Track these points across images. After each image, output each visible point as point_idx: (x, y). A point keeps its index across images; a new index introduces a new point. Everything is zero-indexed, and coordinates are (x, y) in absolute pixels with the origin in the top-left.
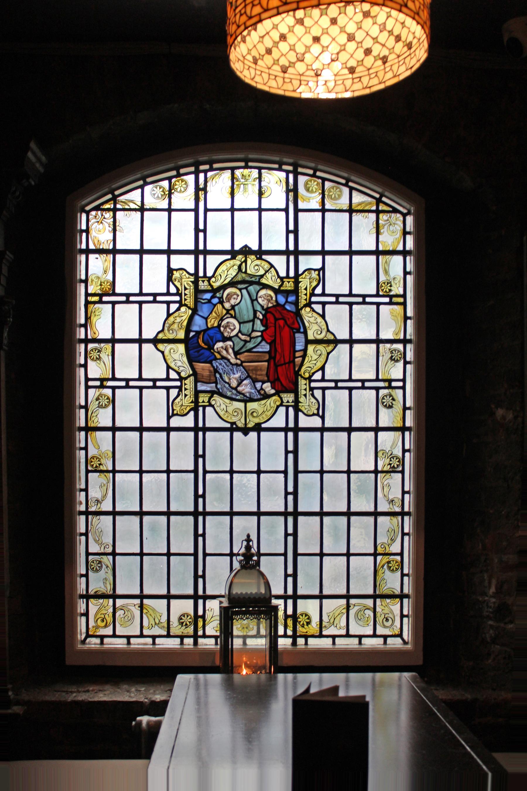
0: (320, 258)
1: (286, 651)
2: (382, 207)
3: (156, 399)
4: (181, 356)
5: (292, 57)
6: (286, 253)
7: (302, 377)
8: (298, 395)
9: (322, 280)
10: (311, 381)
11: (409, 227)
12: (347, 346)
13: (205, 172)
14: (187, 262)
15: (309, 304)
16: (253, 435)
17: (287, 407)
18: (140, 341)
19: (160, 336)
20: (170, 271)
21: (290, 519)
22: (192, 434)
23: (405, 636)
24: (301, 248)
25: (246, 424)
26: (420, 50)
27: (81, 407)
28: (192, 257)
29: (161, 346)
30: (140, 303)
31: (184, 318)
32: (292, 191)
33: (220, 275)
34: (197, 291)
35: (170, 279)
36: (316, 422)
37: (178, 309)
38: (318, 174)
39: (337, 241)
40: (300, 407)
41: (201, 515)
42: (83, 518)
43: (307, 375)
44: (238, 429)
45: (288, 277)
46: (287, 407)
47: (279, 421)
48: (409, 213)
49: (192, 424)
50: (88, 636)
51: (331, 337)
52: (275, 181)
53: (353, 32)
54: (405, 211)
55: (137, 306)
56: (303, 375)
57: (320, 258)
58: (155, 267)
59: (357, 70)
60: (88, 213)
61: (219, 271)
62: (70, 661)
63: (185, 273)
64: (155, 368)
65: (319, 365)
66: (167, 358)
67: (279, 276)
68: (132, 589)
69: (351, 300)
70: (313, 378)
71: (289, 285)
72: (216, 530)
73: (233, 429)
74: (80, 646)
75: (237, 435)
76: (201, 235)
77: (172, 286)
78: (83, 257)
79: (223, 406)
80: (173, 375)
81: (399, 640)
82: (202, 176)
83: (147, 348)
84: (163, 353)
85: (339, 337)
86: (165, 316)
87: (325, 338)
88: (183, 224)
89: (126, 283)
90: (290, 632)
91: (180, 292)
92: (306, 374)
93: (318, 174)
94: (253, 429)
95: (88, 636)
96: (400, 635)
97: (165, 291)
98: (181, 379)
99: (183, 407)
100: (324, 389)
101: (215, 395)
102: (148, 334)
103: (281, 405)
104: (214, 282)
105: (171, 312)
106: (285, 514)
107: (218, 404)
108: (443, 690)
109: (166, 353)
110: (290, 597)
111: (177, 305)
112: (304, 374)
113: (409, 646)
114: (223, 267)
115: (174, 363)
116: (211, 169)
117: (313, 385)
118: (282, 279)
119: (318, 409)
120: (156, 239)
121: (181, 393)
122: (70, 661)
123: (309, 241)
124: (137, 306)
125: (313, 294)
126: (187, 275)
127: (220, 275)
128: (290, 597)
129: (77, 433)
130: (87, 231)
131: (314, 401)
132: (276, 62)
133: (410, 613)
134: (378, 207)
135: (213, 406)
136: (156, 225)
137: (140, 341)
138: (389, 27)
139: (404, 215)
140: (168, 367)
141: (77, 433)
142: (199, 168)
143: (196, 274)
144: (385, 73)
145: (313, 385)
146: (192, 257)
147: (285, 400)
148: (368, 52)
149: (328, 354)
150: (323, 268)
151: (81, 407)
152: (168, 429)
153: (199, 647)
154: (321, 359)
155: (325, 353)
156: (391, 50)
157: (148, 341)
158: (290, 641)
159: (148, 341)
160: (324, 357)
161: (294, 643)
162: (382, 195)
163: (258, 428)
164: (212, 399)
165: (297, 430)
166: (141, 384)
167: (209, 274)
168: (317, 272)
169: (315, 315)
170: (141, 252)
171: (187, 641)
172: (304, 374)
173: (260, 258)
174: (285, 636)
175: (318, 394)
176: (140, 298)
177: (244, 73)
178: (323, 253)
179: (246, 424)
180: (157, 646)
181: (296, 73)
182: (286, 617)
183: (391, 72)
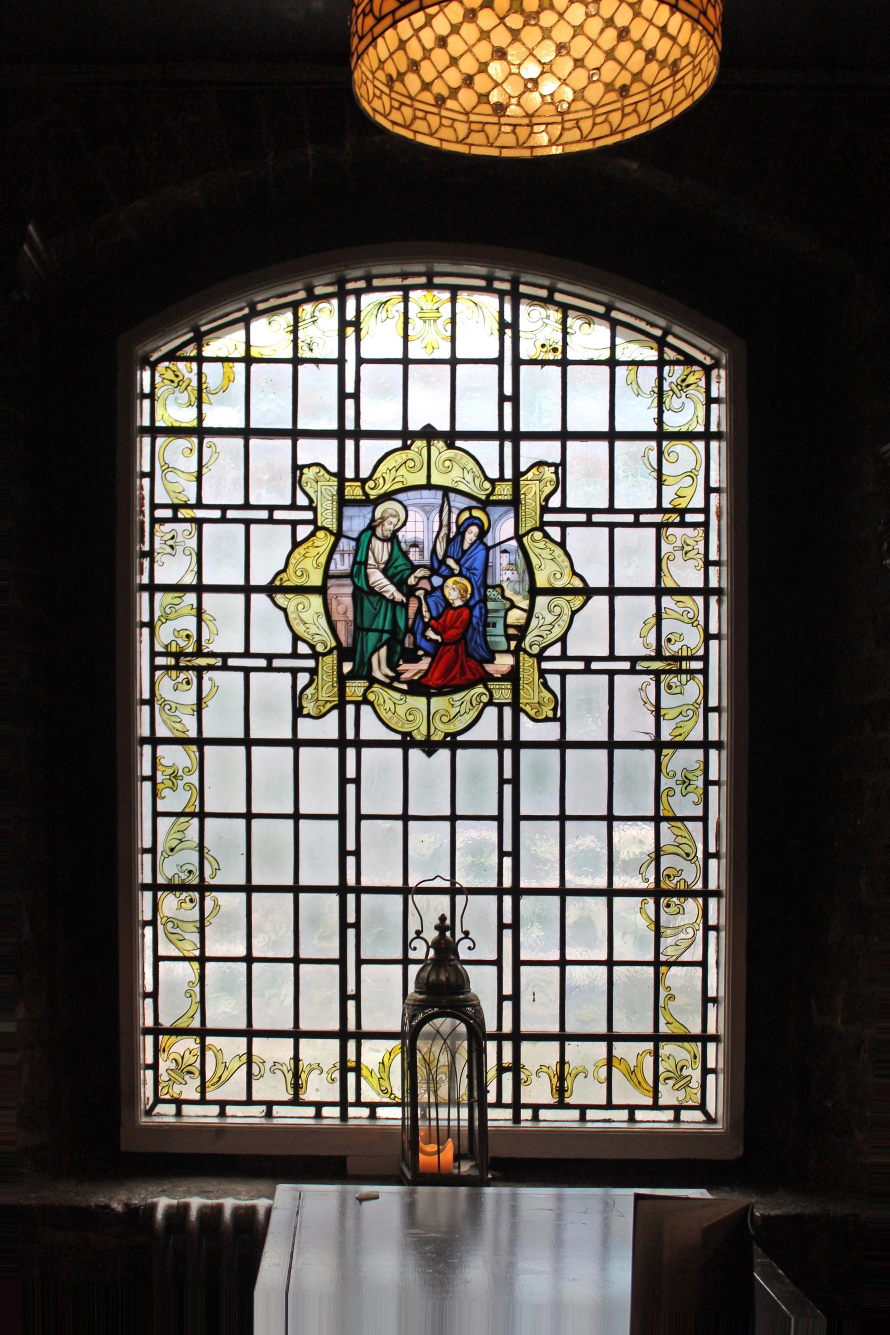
0: (301, 735)
1: (501, 1133)
2: (670, 355)
3: (273, 689)
4: (316, 616)
6: (499, 436)
7: (526, 652)
8: (519, 685)
9: (561, 483)
10: (314, 522)
11: (719, 389)
12: (605, 599)
13: (358, 293)
14: (324, 452)
15: (542, 526)
16: (444, 754)
17: (357, 478)
18: (247, 590)
19: (578, 601)
20: (297, 469)
21: (508, 900)
22: (334, 752)
23: (711, 1107)
24: (523, 428)
25: (429, 735)
28: (333, 443)
29: (280, 598)
30: (612, 657)
31: (321, 550)
32: (509, 327)
33: (384, 478)
34: (343, 502)
35: (296, 482)
36: (551, 732)
37: (313, 534)
38: (558, 297)
39: (588, 414)
40: (521, 705)
41: (351, 892)
42: (148, 896)
43: (535, 650)
44: (441, 435)
45: (358, 705)
46: (500, 706)
47: (486, 730)
48: (717, 365)
49: (334, 735)
50: (158, 1100)
51: (578, 583)
52: (479, 314)
54: (708, 361)
55: (618, 653)
56: (528, 649)
57: (557, 444)
58: (585, 724)
59: (632, 91)
60: (153, 366)
61: (473, 714)
62: (125, 1146)
63: (323, 472)
64: (271, 636)
65: (557, 632)
66: (567, 563)
67: (487, 478)
68: (242, 1000)
69: (607, 518)
70: (546, 654)
71: (355, 689)
72: (381, 915)
73: (451, 437)
74: (144, 1120)
75: (415, 754)
76: (508, 774)
77: (300, 495)
78: (147, 441)
79: (389, 705)
80: (555, 533)
81: (698, 1115)
82: (351, 302)
83: (259, 600)
84: (285, 610)
85: (592, 584)
86: (289, 547)
87: (569, 586)
88: (319, 385)
89: (223, 488)
90: (507, 1098)
91: (314, 505)
92: (534, 647)
93: (558, 297)
94: (442, 744)
95: (158, 1100)
96: (702, 1107)
97: (288, 502)
98: (315, 655)
99: (319, 703)
100: (563, 673)
101: (375, 685)
102: (260, 578)
103: (490, 703)
104: (372, 489)
105: (299, 539)
106: (499, 892)
107: (477, 482)
109: (568, 571)
110: (507, 1037)
111: (310, 528)
112: (530, 647)
113: (719, 1127)
114: (390, 462)
115: (555, 554)
116: (370, 289)
117: (545, 665)
118: (493, 482)
119: (555, 710)
120: (271, 411)
121: (543, 503)
122: (125, 1146)
123: (321, 765)
124: (618, 653)
125: (545, 509)
126: (327, 476)
127: (384, 478)
128: (507, 1037)
130: (152, 396)
131: (548, 695)
132: (483, 98)
134: (661, 353)
135: (371, 704)
136: (271, 383)
137: (247, 590)
139: (707, 371)
140: (562, 545)
142: (344, 287)
143: (340, 475)
145: (545, 665)
146: (333, 443)
147: (496, 695)
148: (650, 55)
149: (574, 613)
150: (564, 462)
152: (564, 436)
153: (351, 1122)
154: (561, 622)
155: (567, 613)
157: (259, 589)
158: (508, 1113)
159: (259, 589)
160: (566, 618)
161: (517, 1119)
162: (666, 332)
163: (453, 743)
164: (488, 492)
165: (517, 745)
166: (249, 662)
167: (364, 474)
168: (552, 469)
169: (550, 545)
170: (611, 745)
171: (326, 1111)
172: (530, 647)
173: (404, 734)
174: (499, 1104)
175: (554, 681)
176: (246, 515)
178: (296, 743)
179: (429, 735)
180: (275, 1121)
181: (407, 94)
182: (501, 1069)
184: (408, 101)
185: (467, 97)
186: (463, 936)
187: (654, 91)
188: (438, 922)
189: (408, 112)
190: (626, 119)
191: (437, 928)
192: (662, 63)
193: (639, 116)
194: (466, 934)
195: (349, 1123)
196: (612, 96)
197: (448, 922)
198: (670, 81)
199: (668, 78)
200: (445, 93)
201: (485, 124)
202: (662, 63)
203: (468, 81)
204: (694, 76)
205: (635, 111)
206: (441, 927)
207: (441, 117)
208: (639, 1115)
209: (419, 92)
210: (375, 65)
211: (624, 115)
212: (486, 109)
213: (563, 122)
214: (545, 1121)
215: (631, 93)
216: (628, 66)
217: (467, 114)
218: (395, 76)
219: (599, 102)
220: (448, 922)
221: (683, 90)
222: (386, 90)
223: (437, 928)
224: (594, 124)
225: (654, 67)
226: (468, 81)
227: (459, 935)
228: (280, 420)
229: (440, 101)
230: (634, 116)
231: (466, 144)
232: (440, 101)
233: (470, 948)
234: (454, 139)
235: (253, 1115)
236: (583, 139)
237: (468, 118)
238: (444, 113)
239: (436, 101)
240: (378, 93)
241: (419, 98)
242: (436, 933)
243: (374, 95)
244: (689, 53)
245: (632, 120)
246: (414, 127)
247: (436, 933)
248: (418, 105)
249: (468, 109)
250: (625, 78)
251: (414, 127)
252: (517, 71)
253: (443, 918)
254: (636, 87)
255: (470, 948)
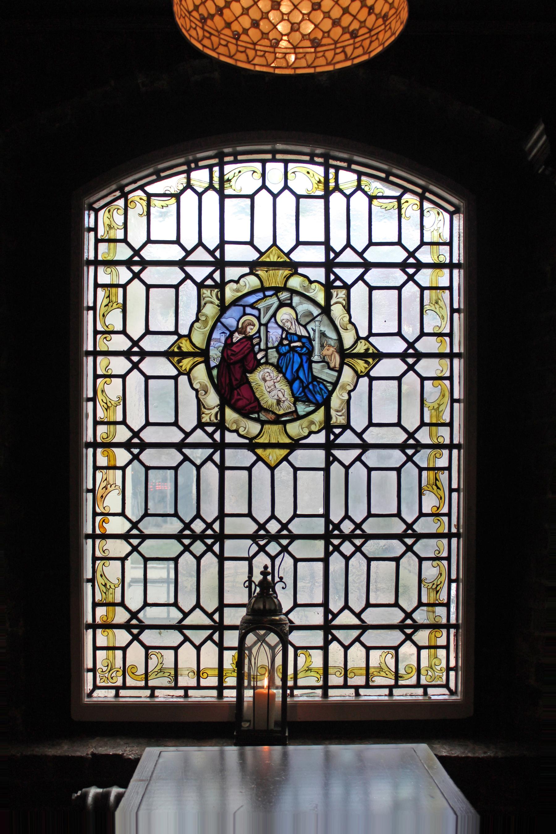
5: (246, 22)
26: (397, 22)
27: (458, 401)
53: (250, 21)
60: (97, 211)
108: (137, 747)
129: (462, 442)
133: (121, 699)
138: (252, 32)
141: (462, 442)
144: (336, 54)
151: (458, 401)
156: (363, 23)
177: (190, 32)
181: (251, 42)
183: (377, 41)
184: (216, 33)
185: (218, 22)
186: (279, 580)
187: (373, 33)
188: (263, 569)
189: (215, 39)
190: (356, 51)
191: (262, 573)
192: (378, 16)
193: (363, 48)
194: (281, 578)
195: (329, 699)
196: (347, 36)
197: (269, 570)
198: (383, 27)
199: (382, 25)
200: (240, 31)
201: (265, 52)
202: (378, 16)
203: (255, 24)
204: (397, 22)
205: (361, 45)
206: (264, 573)
207: (220, 38)
208: (191, 692)
209: (223, 29)
210: (191, 8)
211: (355, 48)
212: (266, 42)
213: (315, 52)
214: (227, 697)
215: (359, 34)
216: (357, 17)
217: (255, 44)
218: (206, 15)
219: (338, 40)
220: (269, 570)
221: (389, 31)
222: (200, 25)
223: (262, 573)
224: (336, 54)
225: (373, 17)
226: (255, 24)
227: (277, 579)
228: (170, 239)
229: (237, 36)
230: (361, 48)
231: (234, 59)
232: (237, 36)
233: (283, 588)
234: (228, 54)
235: (348, 695)
236: (328, 64)
237: (237, 42)
238: (239, 43)
239: (234, 35)
240: (194, 26)
241: (223, 32)
242: (261, 577)
243: (191, 27)
244: (394, 7)
245: (360, 51)
246: (235, 57)
247: (261, 577)
248: (222, 36)
249: (255, 42)
250: (355, 25)
251: (235, 57)
252: (287, 18)
253: (266, 567)
254: (363, 31)
255: (283, 588)
